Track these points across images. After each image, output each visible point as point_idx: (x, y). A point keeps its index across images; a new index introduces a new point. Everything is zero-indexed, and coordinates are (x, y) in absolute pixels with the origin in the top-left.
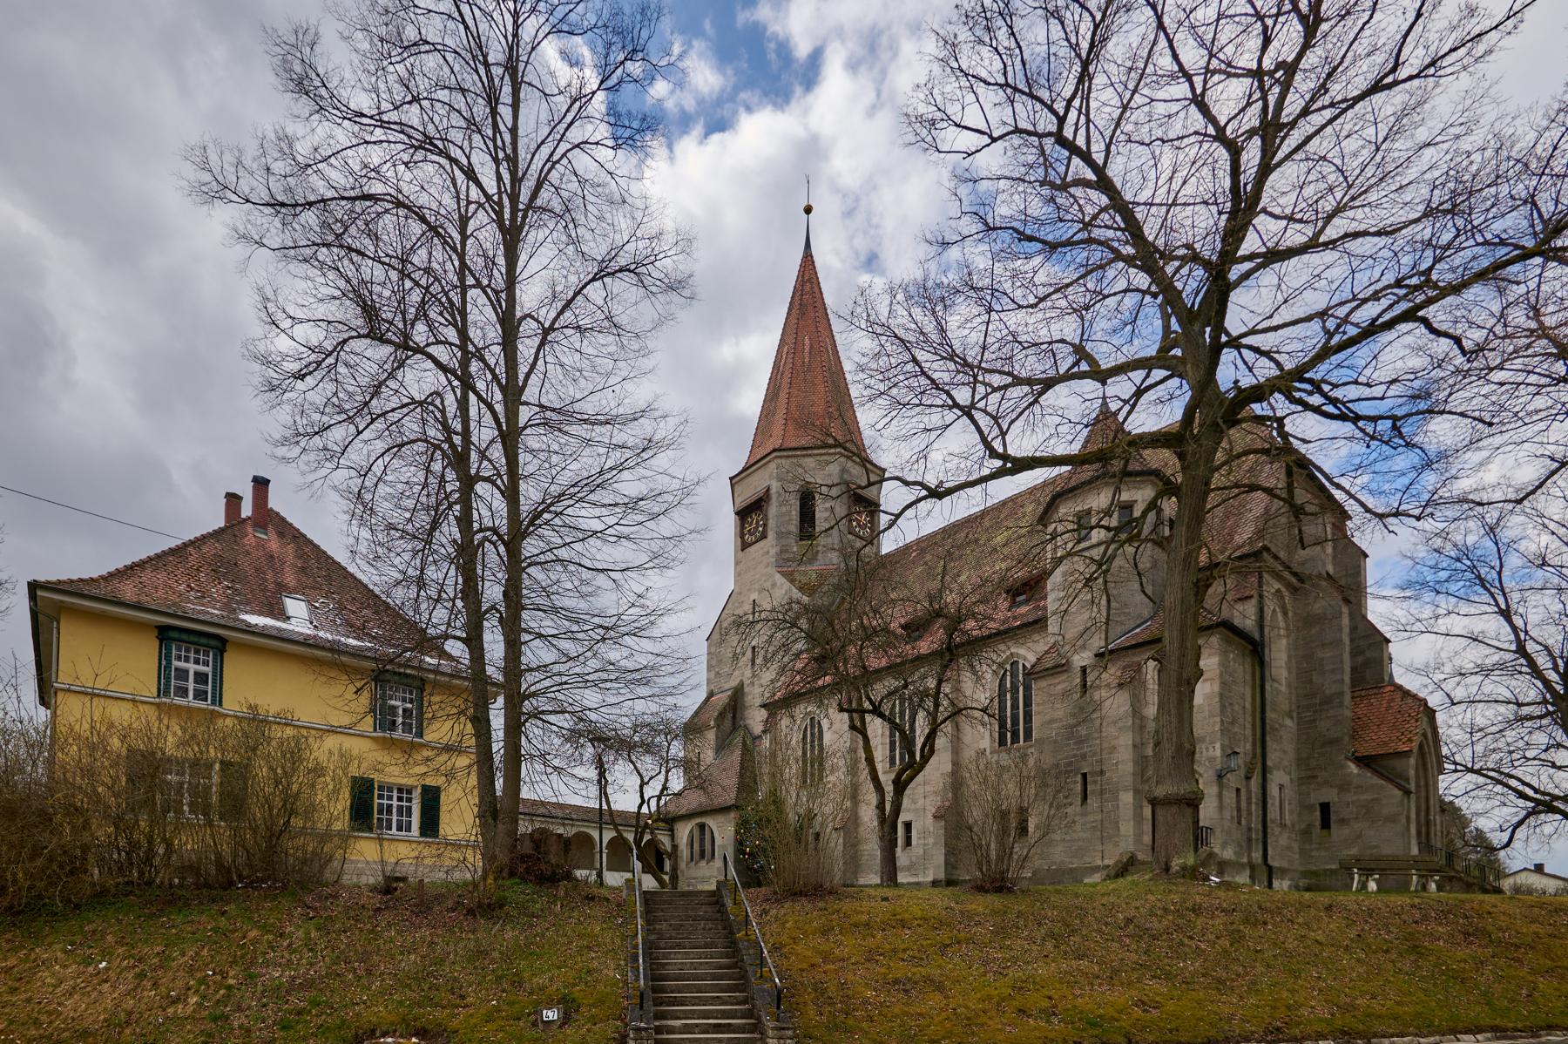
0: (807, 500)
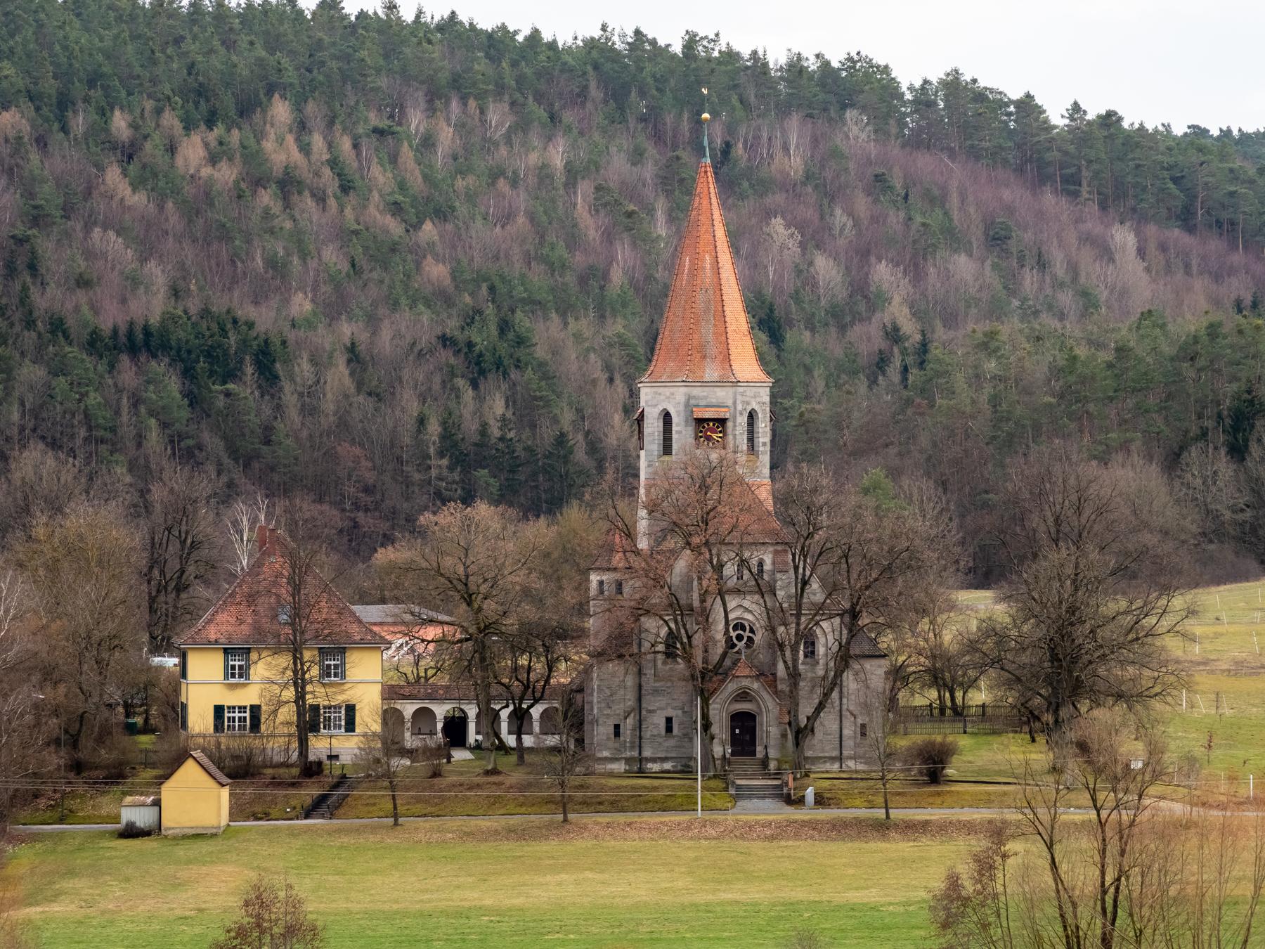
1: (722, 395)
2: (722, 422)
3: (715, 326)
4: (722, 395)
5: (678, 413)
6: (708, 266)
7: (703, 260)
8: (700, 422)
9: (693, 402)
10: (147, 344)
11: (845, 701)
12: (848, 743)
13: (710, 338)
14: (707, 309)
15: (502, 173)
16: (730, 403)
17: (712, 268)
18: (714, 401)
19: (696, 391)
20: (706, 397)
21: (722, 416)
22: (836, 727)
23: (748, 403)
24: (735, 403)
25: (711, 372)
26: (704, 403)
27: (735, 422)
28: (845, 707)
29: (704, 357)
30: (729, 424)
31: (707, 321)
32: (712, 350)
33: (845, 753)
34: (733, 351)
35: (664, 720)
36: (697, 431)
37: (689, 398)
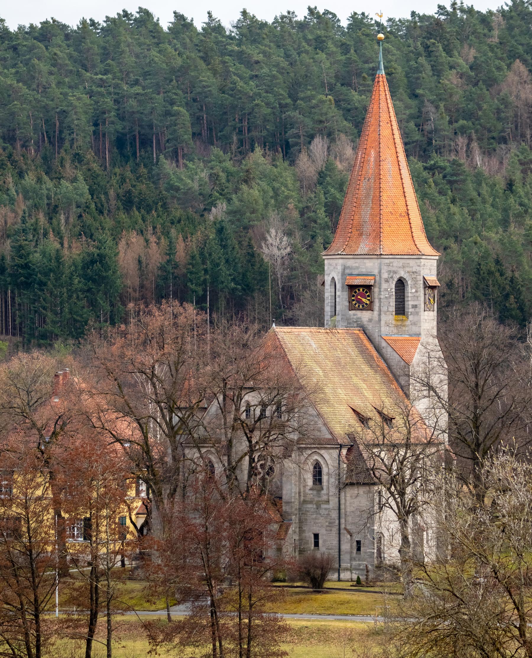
0: (401, 284)
1: (370, 265)
2: (369, 288)
3: (372, 208)
4: (370, 265)
5: (338, 279)
6: (372, 159)
7: (369, 155)
8: (352, 288)
9: (347, 271)
10: (169, 254)
11: (343, 521)
12: (345, 557)
13: (367, 218)
14: (367, 196)
15: (499, 111)
16: (376, 272)
17: (375, 161)
18: (364, 271)
19: (351, 263)
20: (357, 268)
21: (367, 283)
22: (335, 542)
23: (395, 272)
24: (380, 272)
25: (363, 247)
26: (356, 272)
27: (380, 288)
28: (343, 526)
29: (361, 234)
30: (376, 290)
31: (367, 205)
32: (368, 228)
33: (343, 565)
34: (386, 229)
35: (313, 536)
36: (351, 296)
37: (345, 268)
